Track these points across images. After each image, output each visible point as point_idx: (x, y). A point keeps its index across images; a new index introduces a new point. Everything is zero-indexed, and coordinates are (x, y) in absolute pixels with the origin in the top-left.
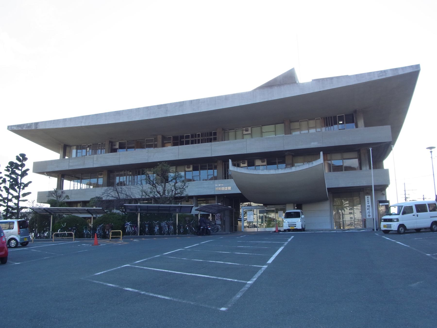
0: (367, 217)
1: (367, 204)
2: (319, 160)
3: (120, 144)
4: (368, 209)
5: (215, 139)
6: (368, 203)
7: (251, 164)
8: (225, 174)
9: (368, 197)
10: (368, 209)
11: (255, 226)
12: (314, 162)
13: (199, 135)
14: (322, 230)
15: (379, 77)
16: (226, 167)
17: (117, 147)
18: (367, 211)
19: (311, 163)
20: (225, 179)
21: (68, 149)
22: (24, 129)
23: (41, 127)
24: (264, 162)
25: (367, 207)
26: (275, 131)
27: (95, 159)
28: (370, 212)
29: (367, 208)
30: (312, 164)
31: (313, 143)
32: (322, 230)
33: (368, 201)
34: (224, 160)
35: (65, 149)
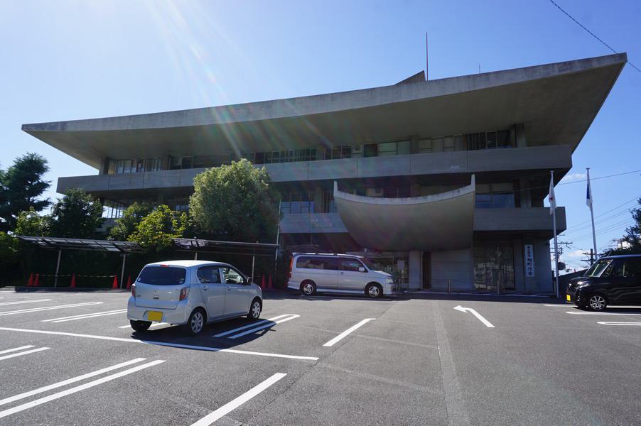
0: (528, 275)
1: (527, 257)
2: (469, 186)
3: (184, 159)
4: (528, 264)
5: (313, 159)
6: (529, 256)
7: (361, 193)
8: (325, 206)
9: (529, 247)
10: (528, 264)
11: (557, 257)
12: (461, 189)
13: (291, 152)
14: (337, 289)
15: (560, 71)
16: (328, 197)
17: (180, 163)
18: (527, 267)
19: (456, 190)
20: (325, 212)
21: (112, 164)
22: (46, 130)
23: (70, 128)
24: (379, 192)
25: (526, 259)
26: (397, 151)
27: (146, 177)
28: (531, 268)
29: (527, 262)
30: (459, 191)
31: (452, 167)
32: (337, 289)
33: (529, 253)
34: (326, 186)
35: (105, 161)
